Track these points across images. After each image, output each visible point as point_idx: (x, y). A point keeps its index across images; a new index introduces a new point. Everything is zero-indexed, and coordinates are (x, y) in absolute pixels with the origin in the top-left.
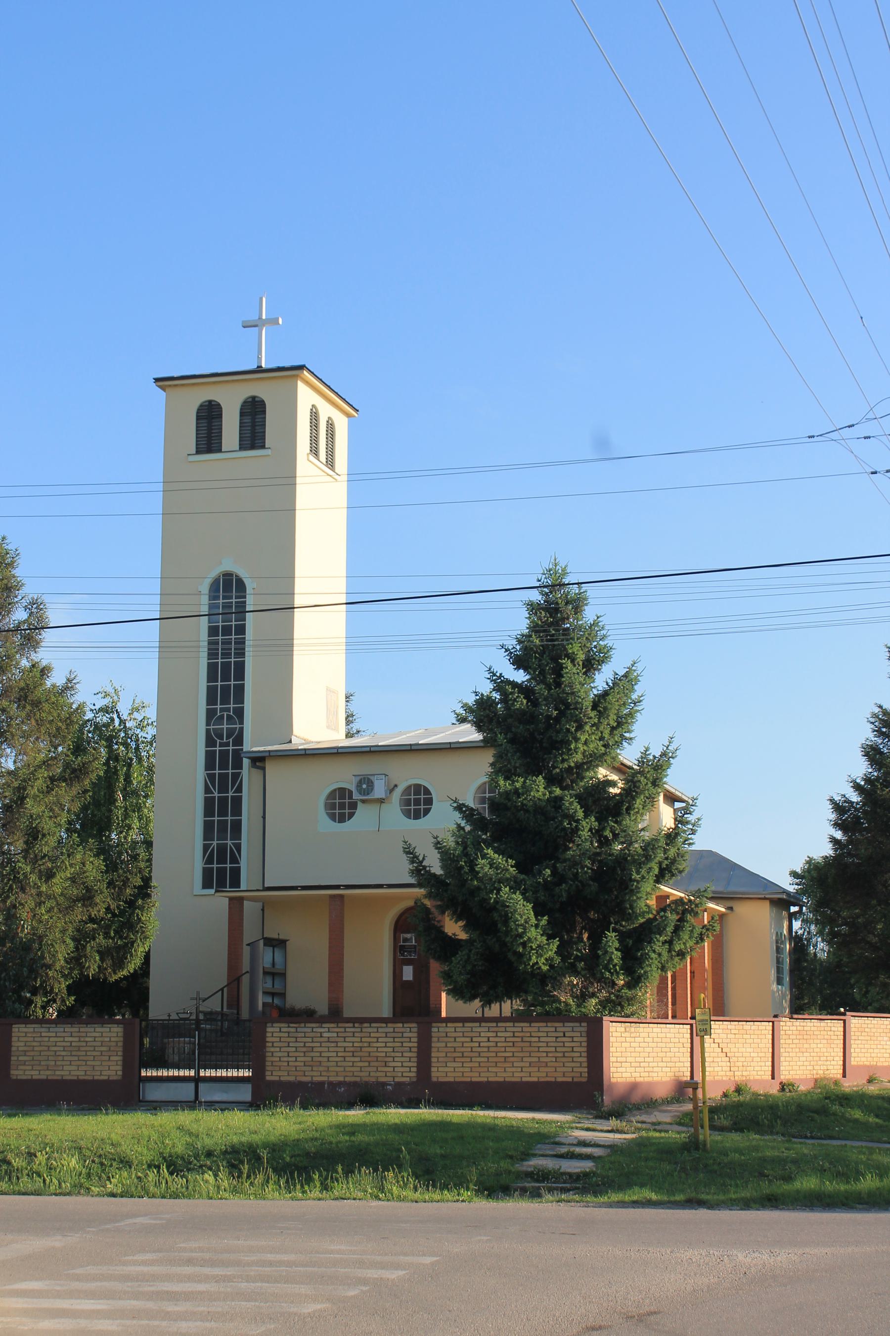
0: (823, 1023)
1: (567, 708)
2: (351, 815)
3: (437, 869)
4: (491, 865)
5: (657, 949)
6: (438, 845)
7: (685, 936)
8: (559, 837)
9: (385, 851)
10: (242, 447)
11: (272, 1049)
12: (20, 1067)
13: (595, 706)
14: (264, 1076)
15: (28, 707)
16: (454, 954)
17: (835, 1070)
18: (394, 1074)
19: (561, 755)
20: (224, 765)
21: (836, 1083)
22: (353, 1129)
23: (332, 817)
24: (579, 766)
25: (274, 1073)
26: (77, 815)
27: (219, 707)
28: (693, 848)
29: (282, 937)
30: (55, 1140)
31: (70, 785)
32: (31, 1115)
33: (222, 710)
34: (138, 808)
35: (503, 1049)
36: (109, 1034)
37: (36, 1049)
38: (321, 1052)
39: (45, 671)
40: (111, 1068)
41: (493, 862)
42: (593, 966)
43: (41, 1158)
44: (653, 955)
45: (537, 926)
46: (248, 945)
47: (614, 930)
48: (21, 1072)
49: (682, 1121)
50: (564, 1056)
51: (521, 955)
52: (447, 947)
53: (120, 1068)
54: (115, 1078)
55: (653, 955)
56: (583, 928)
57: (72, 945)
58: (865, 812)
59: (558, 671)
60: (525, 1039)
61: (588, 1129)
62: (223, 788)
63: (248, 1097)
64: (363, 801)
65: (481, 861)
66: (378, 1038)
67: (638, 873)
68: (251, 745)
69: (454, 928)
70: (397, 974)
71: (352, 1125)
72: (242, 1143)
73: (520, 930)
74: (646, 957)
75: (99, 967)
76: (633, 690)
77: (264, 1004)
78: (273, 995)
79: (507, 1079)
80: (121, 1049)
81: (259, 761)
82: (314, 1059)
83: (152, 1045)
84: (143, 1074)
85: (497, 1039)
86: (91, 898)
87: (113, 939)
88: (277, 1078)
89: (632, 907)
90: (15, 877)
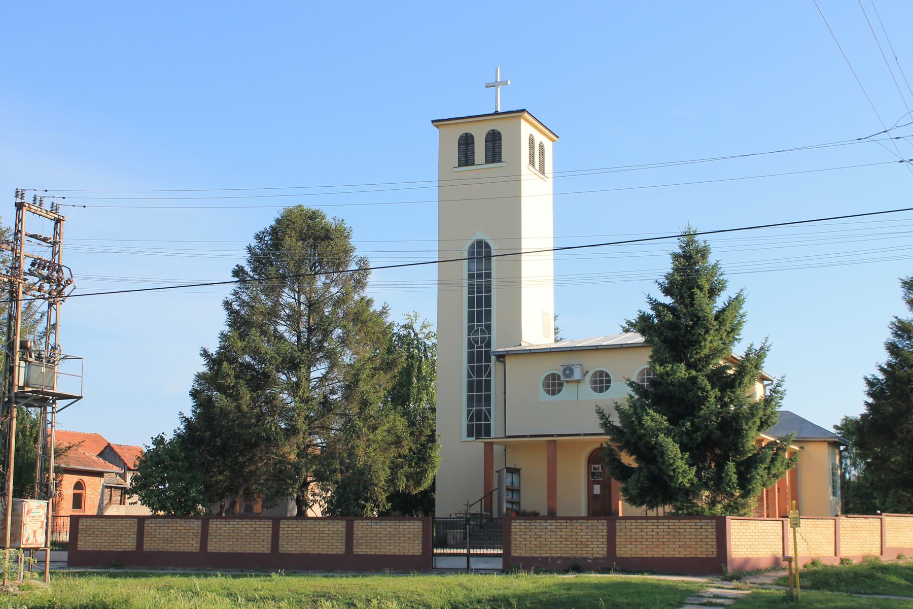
0: (867, 521)
1: (698, 320)
2: (559, 391)
3: (616, 421)
4: (652, 420)
5: (761, 473)
6: (617, 408)
7: (778, 464)
9: (582, 414)
10: (486, 162)
13: (717, 318)
15: (359, 325)
16: (630, 476)
17: (876, 551)
21: (876, 558)
22: (569, 587)
23: (548, 392)
24: (707, 357)
26: (389, 392)
28: (781, 409)
30: (383, 592)
31: (385, 373)
32: (367, 576)
34: (426, 388)
39: (369, 302)
41: (654, 419)
42: (718, 484)
44: (758, 477)
45: (682, 459)
47: (733, 461)
49: (780, 582)
51: (672, 477)
52: (624, 473)
55: (758, 477)
56: (711, 460)
57: (389, 471)
58: (888, 386)
59: (692, 296)
61: (718, 588)
62: (479, 375)
63: (500, 566)
64: (567, 382)
65: (645, 417)
67: (747, 425)
69: (628, 460)
71: (569, 584)
72: (499, 595)
74: (753, 478)
76: (741, 308)
77: (507, 509)
78: (512, 503)
81: (501, 357)
83: (439, 535)
84: (435, 551)
89: (743, 447)
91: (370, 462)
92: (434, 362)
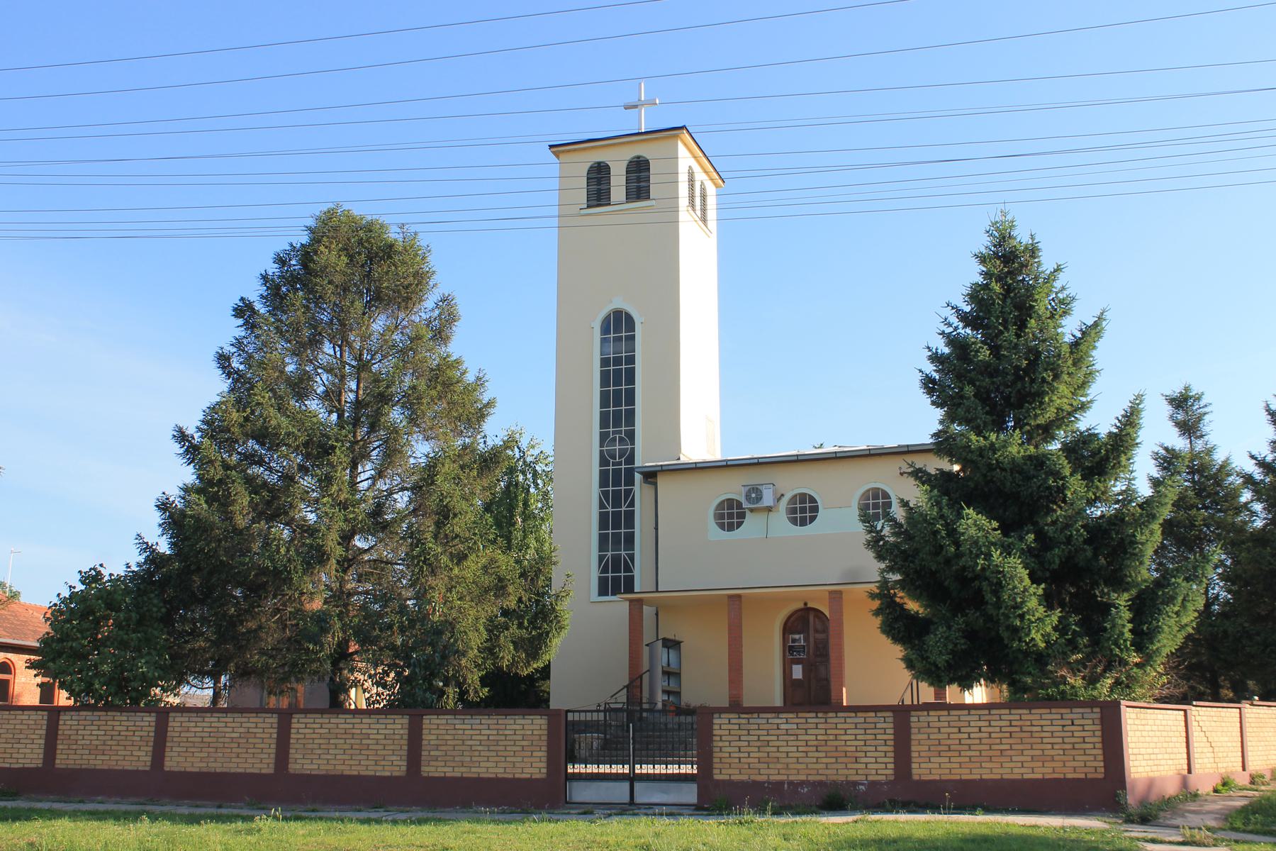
2: (739, 525)
8: (1041, 497)
11: (721, 744)
14: (711, 774)
18: (866, 772)
19: (1034, 409)
23: (722, 526)
34: (537, 529)
44: (1166, 628)
48: (433, 769)
51: (1015, 630)
54: (538, 776)
57: (485, 635)
62: (616, 503)
63: (693, 799)
70: (787, 673)
81: (651, 476)
84: (570, 771)
85: (990, 729)
86: (504, 588)
88: (727, 777)
91: (454, 614)
92: (546, 493)
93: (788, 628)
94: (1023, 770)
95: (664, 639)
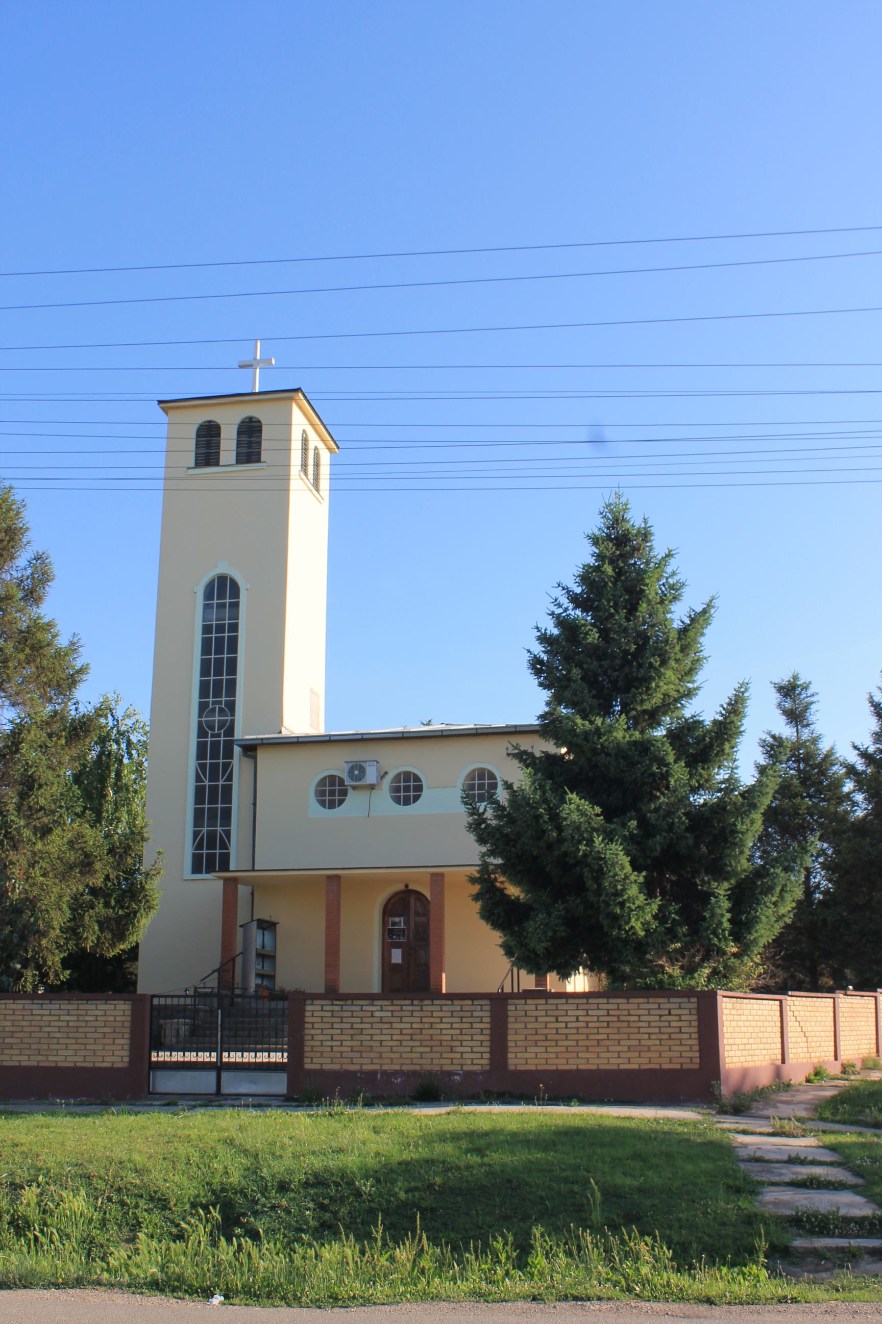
2: (341, 802)
10: (239, 461)
11: (313, 1032)
12: (6, 1051)
14: (302, 1064)
15: (28, 651)
19: (641, 694)
20: (215, 755)
22: (479, 1141)
23: (322, 803)
25: (315, 1060)
27: (211, 700)
29: (273, 919)
33: (214, 703)
34: (128, 802)
35: (595, 1031)
36: (114, 1013)
37: (26, 1029)
38: (372, 1035)
40: (116, 1053)
43: (30, 1194)
44: (763, 918)
46: (241, 926)
48: (7, 1058)
50: (670, 1039)
51: (615, 918)
53: (126, 1053)
54: (120, 1065)
57: (68, 914)
60: (622, 1018)
62: (214, 777)
66: (441, 1018)
68: (243, 732)
72: (327, 1169)
73: (619, 887)
75: (98, 938)
77: (257, 985)
79: (601, 1067)
80: (128, 1030)
81: (250, 749)
82: (364, 1043)
85: (588, 1019)
86: (90, 864)
87: (113, 908)
88: (318, 1067)
90: (6, 831)
91: (36, 891)
93: (389, 910)
94: (619, 1061)
95: (259, 920)
